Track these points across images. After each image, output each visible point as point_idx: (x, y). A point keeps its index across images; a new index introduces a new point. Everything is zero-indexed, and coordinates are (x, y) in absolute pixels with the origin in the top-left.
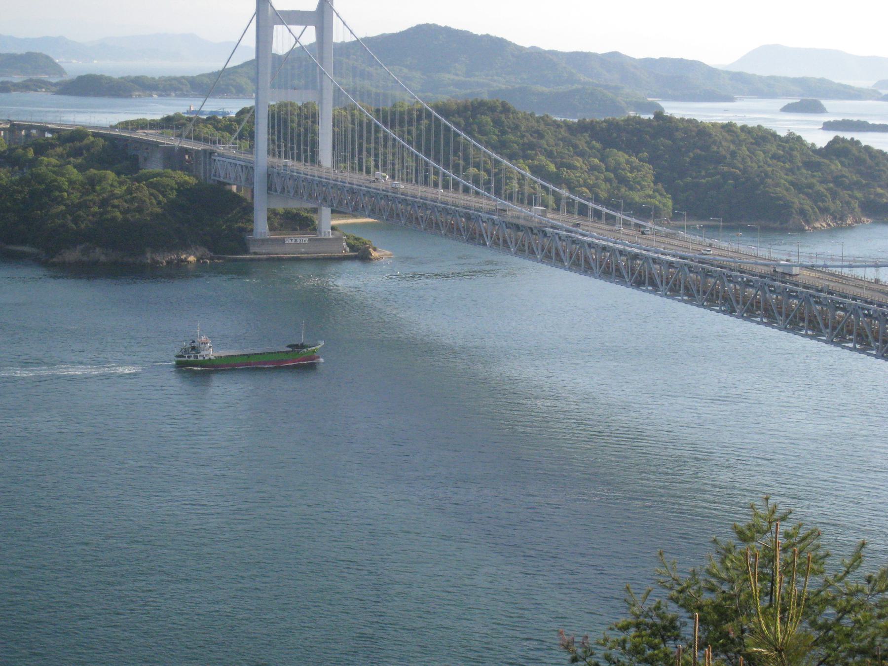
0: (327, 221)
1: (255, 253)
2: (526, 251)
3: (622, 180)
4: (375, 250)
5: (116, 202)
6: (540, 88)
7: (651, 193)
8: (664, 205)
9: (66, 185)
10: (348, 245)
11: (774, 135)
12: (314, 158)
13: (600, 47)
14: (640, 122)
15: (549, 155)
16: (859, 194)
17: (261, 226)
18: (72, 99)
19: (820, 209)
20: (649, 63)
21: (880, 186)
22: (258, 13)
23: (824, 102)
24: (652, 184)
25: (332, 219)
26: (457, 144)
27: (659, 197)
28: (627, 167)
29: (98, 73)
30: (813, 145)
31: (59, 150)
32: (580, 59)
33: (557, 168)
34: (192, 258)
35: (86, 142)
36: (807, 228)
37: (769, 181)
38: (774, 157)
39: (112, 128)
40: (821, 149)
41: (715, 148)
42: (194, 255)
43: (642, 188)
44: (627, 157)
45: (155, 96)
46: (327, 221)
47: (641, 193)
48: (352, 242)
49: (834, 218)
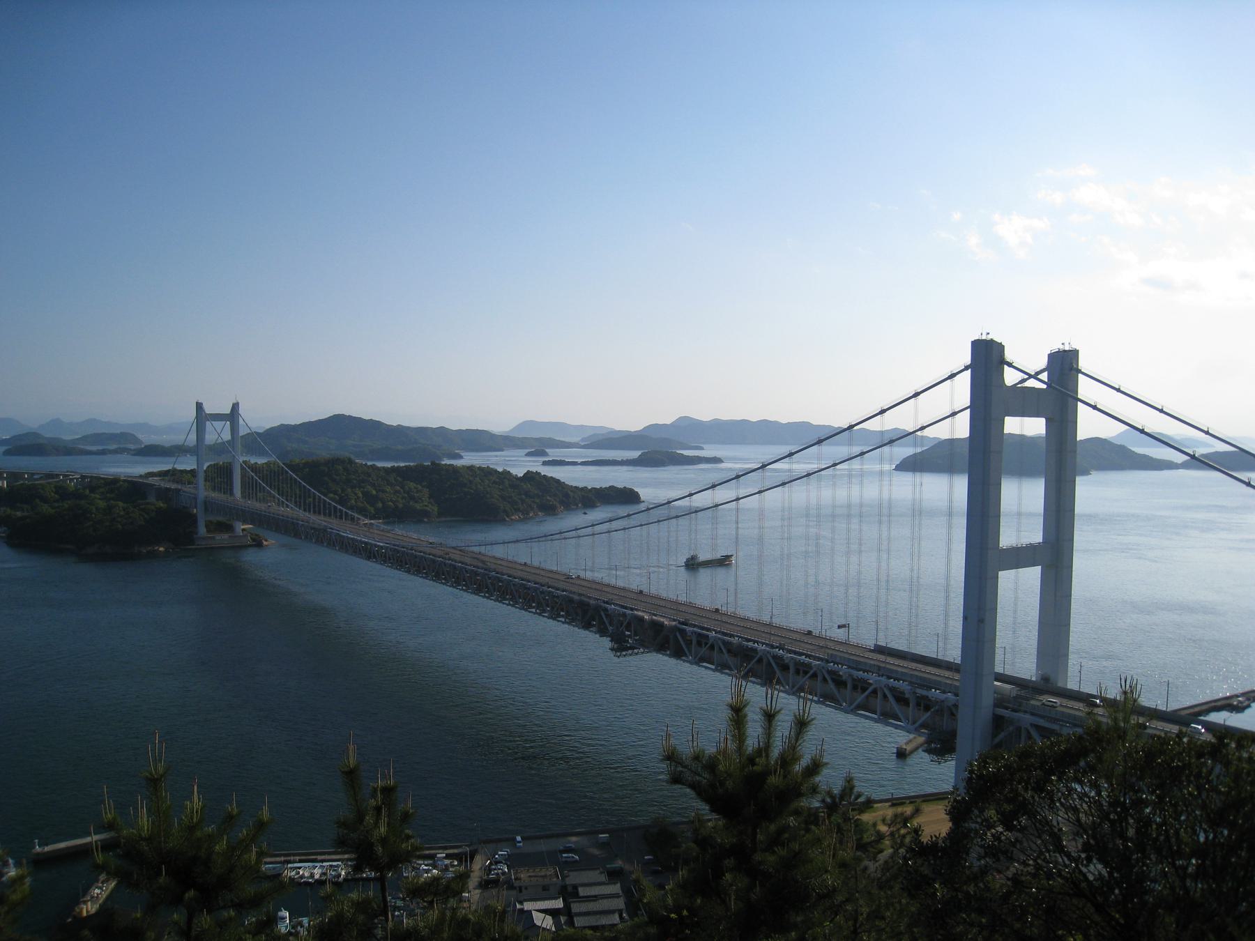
0: (240, 527)
1: (198, 545)
2: (320, 541)
3: (412, 498)
4: (266, 541)
5: (119, 519)
6: (400, 447)
7: (426, 504)
8: (433, 510)
9: (94, 510)
10: (251, 538)
11: (496, 471)
12: (230, 491)
13: (434, 424)
14: (423, 466)
15: (373, 485)
16: (537, 501)
17: (202, 530)
18: (138, 458)
19: (515, 509)
20: (460, 432)
21: (550, 496)
22: (197, 417)
23: (547, 450)
24: (427, 499)
25: (243, 525)
26: (278, 491)
27: (430, 506)
28: (415, 490)
29: (157, 444)
30: (516, 475)
31: (101, 490)
32: (422, 431)
33: (377, 492)
34: (161, 549)
35: (118, 485)
36: (507, 519)
37: (488, 496)
38: (494, 482)
39: (141, 476)
40: (521, 477)
41: (461, 479)
42: (164, 547)
43: (423, 501)
44: (415, 485)
45: (188, 456)
46: (240, 527)
47: (421, 505)
48: (253, 537)
49: (523, 514)
